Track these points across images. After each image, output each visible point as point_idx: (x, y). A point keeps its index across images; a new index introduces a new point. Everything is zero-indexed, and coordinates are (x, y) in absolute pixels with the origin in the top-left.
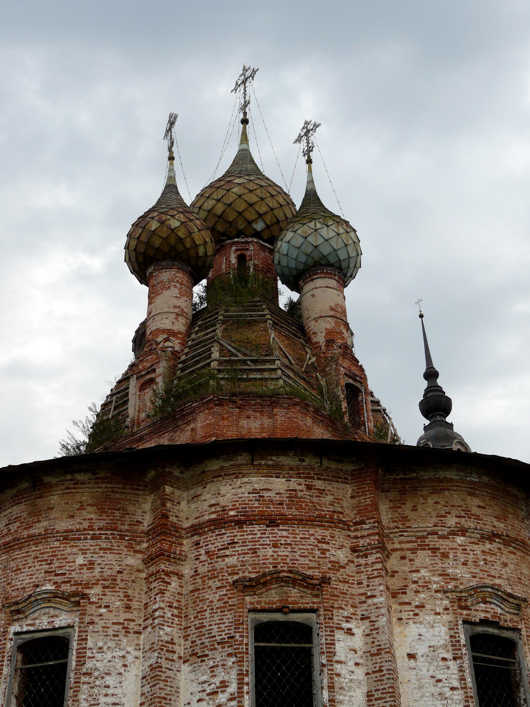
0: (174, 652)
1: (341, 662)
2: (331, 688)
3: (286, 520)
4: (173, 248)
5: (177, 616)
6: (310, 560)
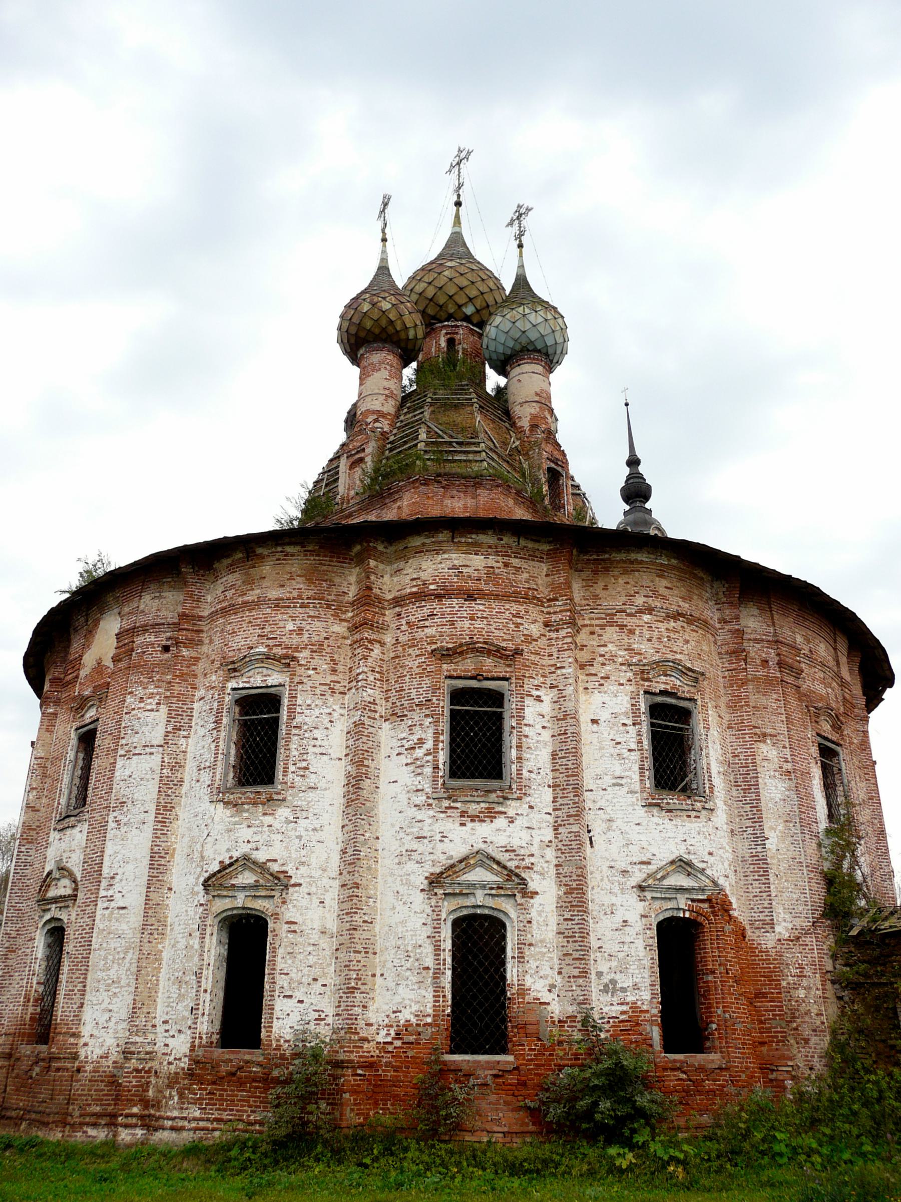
0: (376, 712)
1: (530, 725)
2: (519, 747)
3: (483, 595)
4: (384, 330)
5: (378, 680)
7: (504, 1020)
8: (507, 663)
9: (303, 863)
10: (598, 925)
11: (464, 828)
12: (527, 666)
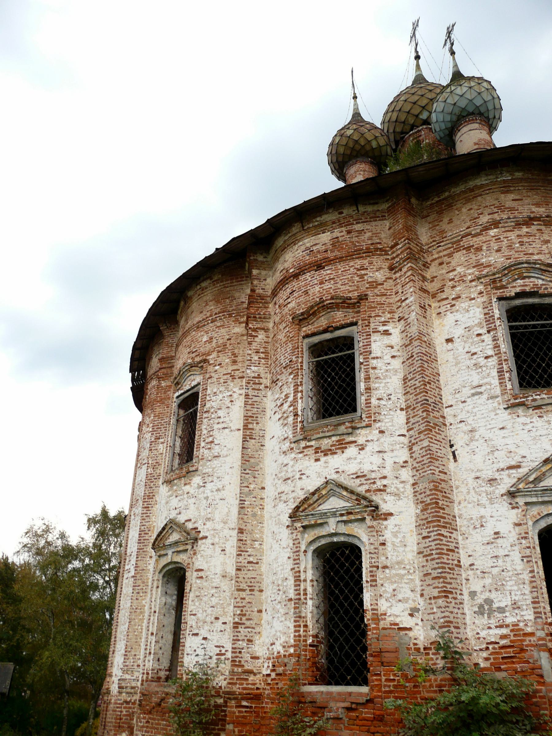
0: (261, 384)
1: (377, 358)
3: (329, 262)
4: (353, 149)
5: (263, 358)
6: (350, 286)
7: (365, 649)
8: (356, 310)
9: (209, 519)
10: (467, 541)
11: (318, 463)
12: (372, 307)
